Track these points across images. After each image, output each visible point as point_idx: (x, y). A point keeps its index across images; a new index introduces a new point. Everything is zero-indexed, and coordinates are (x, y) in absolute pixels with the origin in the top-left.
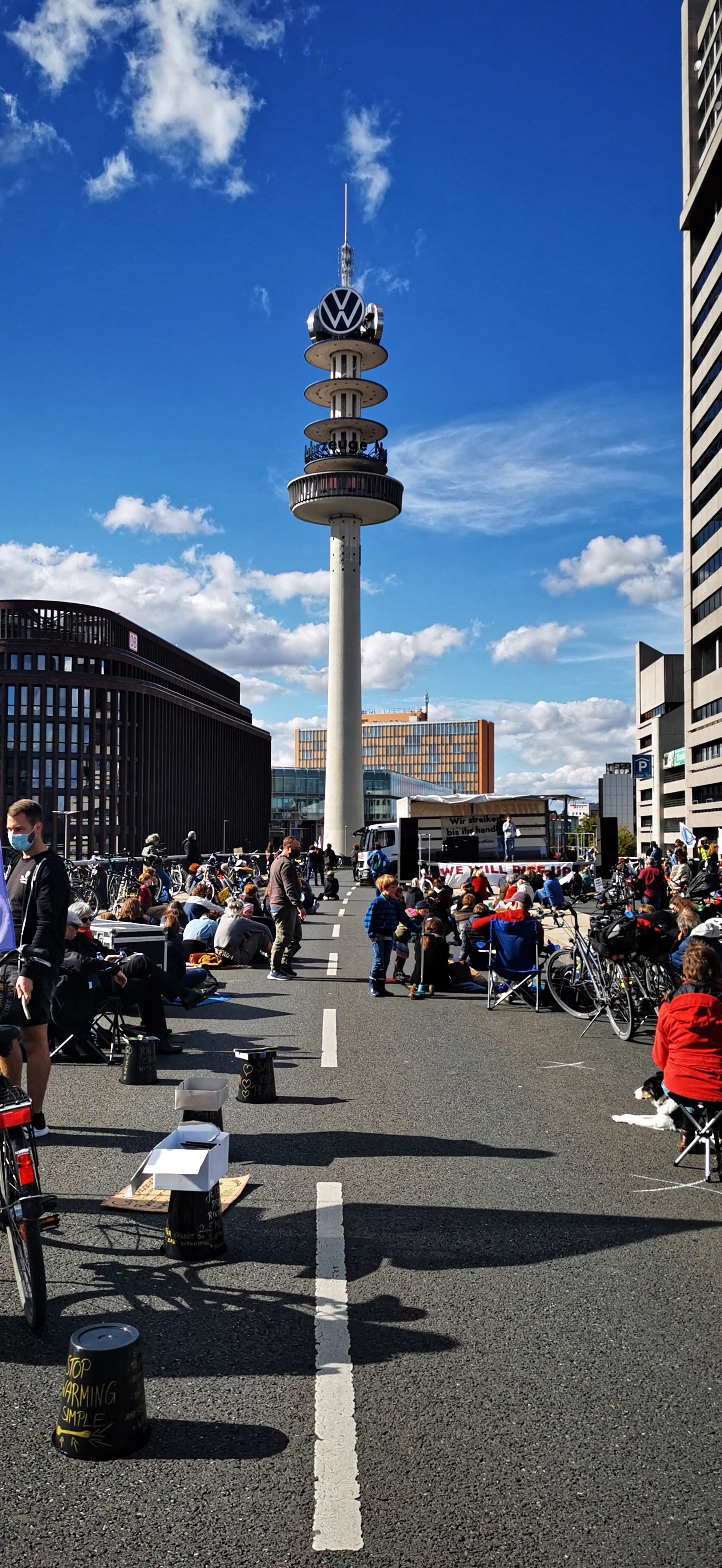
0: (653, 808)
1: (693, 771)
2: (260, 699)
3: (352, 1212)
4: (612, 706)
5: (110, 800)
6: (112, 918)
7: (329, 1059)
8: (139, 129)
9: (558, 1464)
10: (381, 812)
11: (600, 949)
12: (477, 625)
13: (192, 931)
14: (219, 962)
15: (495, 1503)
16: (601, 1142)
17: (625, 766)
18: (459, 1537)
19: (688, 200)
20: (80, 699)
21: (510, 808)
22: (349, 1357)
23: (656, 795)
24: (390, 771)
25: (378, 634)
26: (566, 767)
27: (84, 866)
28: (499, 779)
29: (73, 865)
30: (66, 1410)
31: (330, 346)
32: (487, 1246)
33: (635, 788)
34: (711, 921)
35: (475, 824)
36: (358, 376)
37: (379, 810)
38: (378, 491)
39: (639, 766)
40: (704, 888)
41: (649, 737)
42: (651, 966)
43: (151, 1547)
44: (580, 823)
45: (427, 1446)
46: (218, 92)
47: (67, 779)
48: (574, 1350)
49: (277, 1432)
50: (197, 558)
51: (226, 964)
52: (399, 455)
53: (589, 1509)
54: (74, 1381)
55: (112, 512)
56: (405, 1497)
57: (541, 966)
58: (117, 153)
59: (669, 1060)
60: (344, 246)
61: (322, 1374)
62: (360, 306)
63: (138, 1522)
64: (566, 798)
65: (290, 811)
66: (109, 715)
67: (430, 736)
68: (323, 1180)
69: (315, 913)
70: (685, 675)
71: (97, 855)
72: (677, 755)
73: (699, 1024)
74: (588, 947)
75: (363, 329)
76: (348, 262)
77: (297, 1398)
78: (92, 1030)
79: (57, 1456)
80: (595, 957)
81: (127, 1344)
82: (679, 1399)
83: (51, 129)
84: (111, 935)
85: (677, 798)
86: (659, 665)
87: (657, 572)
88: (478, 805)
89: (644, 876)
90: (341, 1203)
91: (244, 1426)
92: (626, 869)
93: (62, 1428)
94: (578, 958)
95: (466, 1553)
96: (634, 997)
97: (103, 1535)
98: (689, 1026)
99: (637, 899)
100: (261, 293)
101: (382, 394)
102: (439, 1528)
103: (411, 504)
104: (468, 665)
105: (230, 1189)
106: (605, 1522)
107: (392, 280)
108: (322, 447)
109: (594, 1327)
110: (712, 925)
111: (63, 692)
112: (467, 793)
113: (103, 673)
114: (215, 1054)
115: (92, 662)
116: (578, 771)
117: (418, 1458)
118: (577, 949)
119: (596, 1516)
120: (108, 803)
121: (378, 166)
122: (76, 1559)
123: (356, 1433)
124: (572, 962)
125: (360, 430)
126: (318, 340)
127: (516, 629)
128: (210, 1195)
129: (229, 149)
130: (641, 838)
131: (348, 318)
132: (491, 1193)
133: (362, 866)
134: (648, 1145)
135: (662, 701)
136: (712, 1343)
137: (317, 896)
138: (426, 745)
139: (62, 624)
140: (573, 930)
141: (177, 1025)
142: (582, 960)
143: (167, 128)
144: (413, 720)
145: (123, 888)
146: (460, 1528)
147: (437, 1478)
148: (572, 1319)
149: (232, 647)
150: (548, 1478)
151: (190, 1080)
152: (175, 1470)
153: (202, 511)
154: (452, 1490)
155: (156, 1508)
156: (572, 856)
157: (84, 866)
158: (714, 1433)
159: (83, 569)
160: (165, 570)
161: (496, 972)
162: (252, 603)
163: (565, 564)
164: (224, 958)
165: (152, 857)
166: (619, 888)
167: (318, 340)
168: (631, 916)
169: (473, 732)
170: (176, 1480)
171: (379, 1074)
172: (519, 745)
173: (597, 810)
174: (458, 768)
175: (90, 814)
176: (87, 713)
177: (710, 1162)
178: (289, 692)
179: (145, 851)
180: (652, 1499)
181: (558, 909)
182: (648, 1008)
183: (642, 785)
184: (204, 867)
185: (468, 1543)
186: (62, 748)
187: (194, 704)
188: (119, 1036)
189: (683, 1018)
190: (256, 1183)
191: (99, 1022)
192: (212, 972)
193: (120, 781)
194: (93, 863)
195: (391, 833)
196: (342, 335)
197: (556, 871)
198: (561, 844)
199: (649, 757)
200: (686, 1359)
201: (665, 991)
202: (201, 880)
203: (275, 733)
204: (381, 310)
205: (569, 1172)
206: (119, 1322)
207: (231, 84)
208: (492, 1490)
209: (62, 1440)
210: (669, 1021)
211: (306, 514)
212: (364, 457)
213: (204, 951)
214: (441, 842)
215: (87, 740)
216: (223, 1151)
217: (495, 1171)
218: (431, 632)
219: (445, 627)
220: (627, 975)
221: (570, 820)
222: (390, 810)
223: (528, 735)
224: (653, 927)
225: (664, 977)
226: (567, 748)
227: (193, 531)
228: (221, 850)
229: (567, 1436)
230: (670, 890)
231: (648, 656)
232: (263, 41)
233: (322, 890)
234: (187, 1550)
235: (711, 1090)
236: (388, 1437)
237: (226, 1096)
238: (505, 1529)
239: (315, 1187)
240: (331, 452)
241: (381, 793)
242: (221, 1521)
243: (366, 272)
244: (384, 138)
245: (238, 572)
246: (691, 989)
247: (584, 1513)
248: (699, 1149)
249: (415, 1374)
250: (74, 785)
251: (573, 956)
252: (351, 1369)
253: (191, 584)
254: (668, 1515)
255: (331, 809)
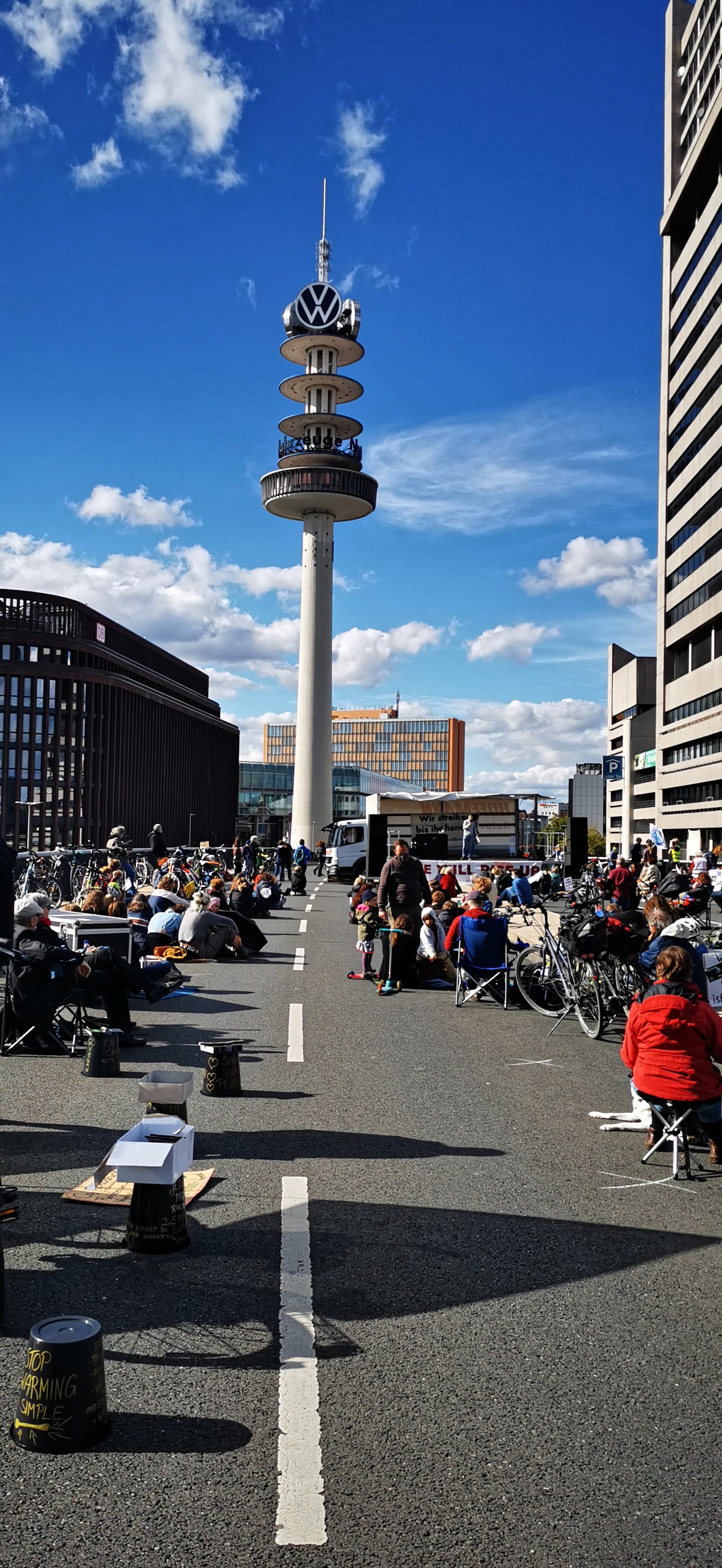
0: (623, 809)
1: (664, 773)
2: (229, 693)
3: (317, 1209)
4: (587, 707)
5: (74, 792)
6: (77, 909)
7: (295, 1054)
8: (129, 118)
9: (524, 1459)
10: (350, 809)
11: (570, 948)
12: (454, 622)
13: (157, 923)
14: (184, 955)
15: (461, 1498)
16: (569, 1139)
17: (596, 766)
18: (424, 1531)
19: (669, 205)
20: (45, 690)
21: (480, 806)
22: (314, 1351)
23: (626, 796)
24: (360, 767)
25: (355, 631)
26: (538, 767)
27: (48, 857)
28: (470, 777)
29: (36, 855)
30: (25, 1402)
31: (306, 341)
32: (454, 1242)
33: (605, 789)
34: (681, 921)
35: (444, 822)
36: (333, 372)
37: (348, 806)
38: (352, 488)
39: (610, 768)
40: (674, 889)
41: (621, 739)
42: (621, 966)
43: (111, 1541)
44: (549, 823)
45: (392, 1440)
46: (211, 81)
47: (31, 770)
48: (540, 1346)
49: (241, 1425)
50: (172, 550)
51: (191, 958)
52: (379, 453)
53: (555, 1504)
54: (33, 1374)
55: (88, 500)
56: (370, 1492)
57: (510, 964)
58: (106, 139)
59: (638, 1059)
60: (322, 241)
61: (286, 1368)
62: (338, 301)
63: (98, 1516)
64: (536, 797)
65: (257, 805)
66: (74, 706)
67: (401, 733)
68: (288, 1175)
69: (281, 908)
70: (658, 678)
71: (60, 846)
72: (648, 757)
73: (671, 1026)
74: (558, 946)
75: (340, 325)
76: (326, 258)
77: (260, 1392)
78: (54, 1022)
79: (15, 1449)
80: (565, 955)
81: (88, 1337)
82: (646, 1395)
83: (43, 114)
84: (75, 927)
85: (647, 800)
86: (632, 667)
87: (637, 575)
88: (448, 803)
89: (614, 877)
90: (307, 1201)
91: (207, 1420)
92: (596, 869)
93: (21, 1421)
94: (548, 957)
95: (431, 1548)
96: (603, 996)
97: (61, 1529)
98: (660, 1027)
99: (606, 899)
100: (248, 284)
101: (359, 390)
102: (404, 1523)
103: (390, 502)
104: (442, 665)
105: (194, 1182)
106: (571, 1517)
107: (382, 277)
108: (296, 442)
109: (561, 1323)
110: (683, 926)
111: (28, 682)
112: (437, 790)
113: (69, 664)
114: (179, 1047)
115: (58, 652)
116: (550, 771)
117: (383, 1453)
118: (547, 948)
119: (562, 1511)
120: (72, 794)
121: (371, 161)
122: (34, 1553)
123: (320, 1427)
124: (542, 960)
125: (335, 426)
126: (294, 334)
127: (493, 628)
128: (174, 1189)
129: (221, 138)
130: (610, 839)
131: (325, 313)
132: (458, 1189)
133: (330, 862)
134: (616, 1142)
135: (633, 702)
136: (679, 1340)
137: (284, 891)
138: (396, 742)
139: (28, 614)
140: (543, 928)
141: (141, 1018)
142: (551, 958)
143: (158, 117)
144: (384, 717)
145: (87, 879)
146: (425, 1523)
147: (402, 1473)
148: (539, 1314)
149: (206, 639)
150: (515, 1473)
151: (154, 1072)
152: (136, 1463)
153: (181, 503)
154: (417, 1485)
155: (116, 1502)
156: (539, 854)
157: (48, 857)
158: (680, 1429)
159: (56, 558)
160: (139, 562)
161: (465, 969)
162: (227, 598)
163: (544, 565)
164: (189, 952)
165: (116, 850)
166: (588, 888)
167: (294, 334)
168: (601, 915)
169: (443, 730)
170: (137, 1473)
171: (346, 1069)
172: (491, 745)
173: (567, 810)
174: (428, 766)
175: (54, 805)
176: (52, 704)
177: (678, 1160)
178: (261, 686)
179: (110, 843)
180: (618, 1494)
181: (528, 907)
182: (616, 1008)
183: (612, 786)
184: (171, 860)
185: (433, 1538)
186: (26, 738)
187: (161, 697)
188: (81, 1028)
189: (653, 1019)
190: (220, 1176)
191: (61, 1014)
192: (177, 965)
193: (85, 772)
194: (57, 854)
195: (359, 830)
196: (318, 330)
197: (525, 871)
198: (530, 843)
199: (620, 758)
200: (653, 1355)
201: (634, 991)
202: (166, 873)
203: (246, 728)
204: (358, 306)
205: (537, 1169)
206: (80, 1314)
207: (225, 73)
208: (458, 1485)
209: (20, 1433)
210: (640, 1021)
211: (279, 508)
212: (339, 453)
213: (168, 944)
214: (410, 839)
215: (51, 731)
216: (187, 1147)
217: (463, 1167)
218: (407, 629)
219: (422, 624)
220: (596, 974)
221: (539, 820)
222: (358, 807)
223: (500, 735)
224: (623, 927)
225: (633, 976)
226: (539, 748)
227: (170, 523)
228: (186, 844)
229: (533, 1431)
230: (639, 890)
231: (621, 658)
232: (260, 32)
233: (289, 885)
234: (147, 1544)
235: (680, 1089)
236: (353, 1432)
237: (191, 1090)
238: (470, 1524)
239: (280, 1181)
240: (306, 447)
241: (350, 789)
242: (183, 1515)
243: (356, 268)
244: (378, 135)
245: (214, 566)
246: (662, 990)
247: (550, 1508)
248: (667, 1147)
249: (380, 1368)
250: (37, 776)
251: (542, 955)
252: (316, 1363)
253: (166, 576)
254: (634, 1510)
255: (299, 804)
